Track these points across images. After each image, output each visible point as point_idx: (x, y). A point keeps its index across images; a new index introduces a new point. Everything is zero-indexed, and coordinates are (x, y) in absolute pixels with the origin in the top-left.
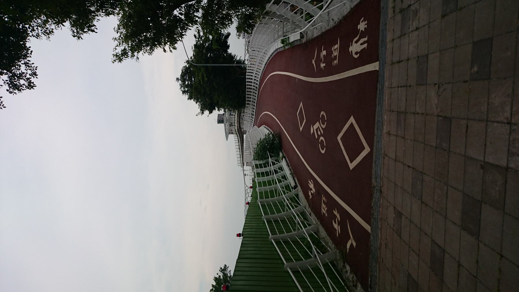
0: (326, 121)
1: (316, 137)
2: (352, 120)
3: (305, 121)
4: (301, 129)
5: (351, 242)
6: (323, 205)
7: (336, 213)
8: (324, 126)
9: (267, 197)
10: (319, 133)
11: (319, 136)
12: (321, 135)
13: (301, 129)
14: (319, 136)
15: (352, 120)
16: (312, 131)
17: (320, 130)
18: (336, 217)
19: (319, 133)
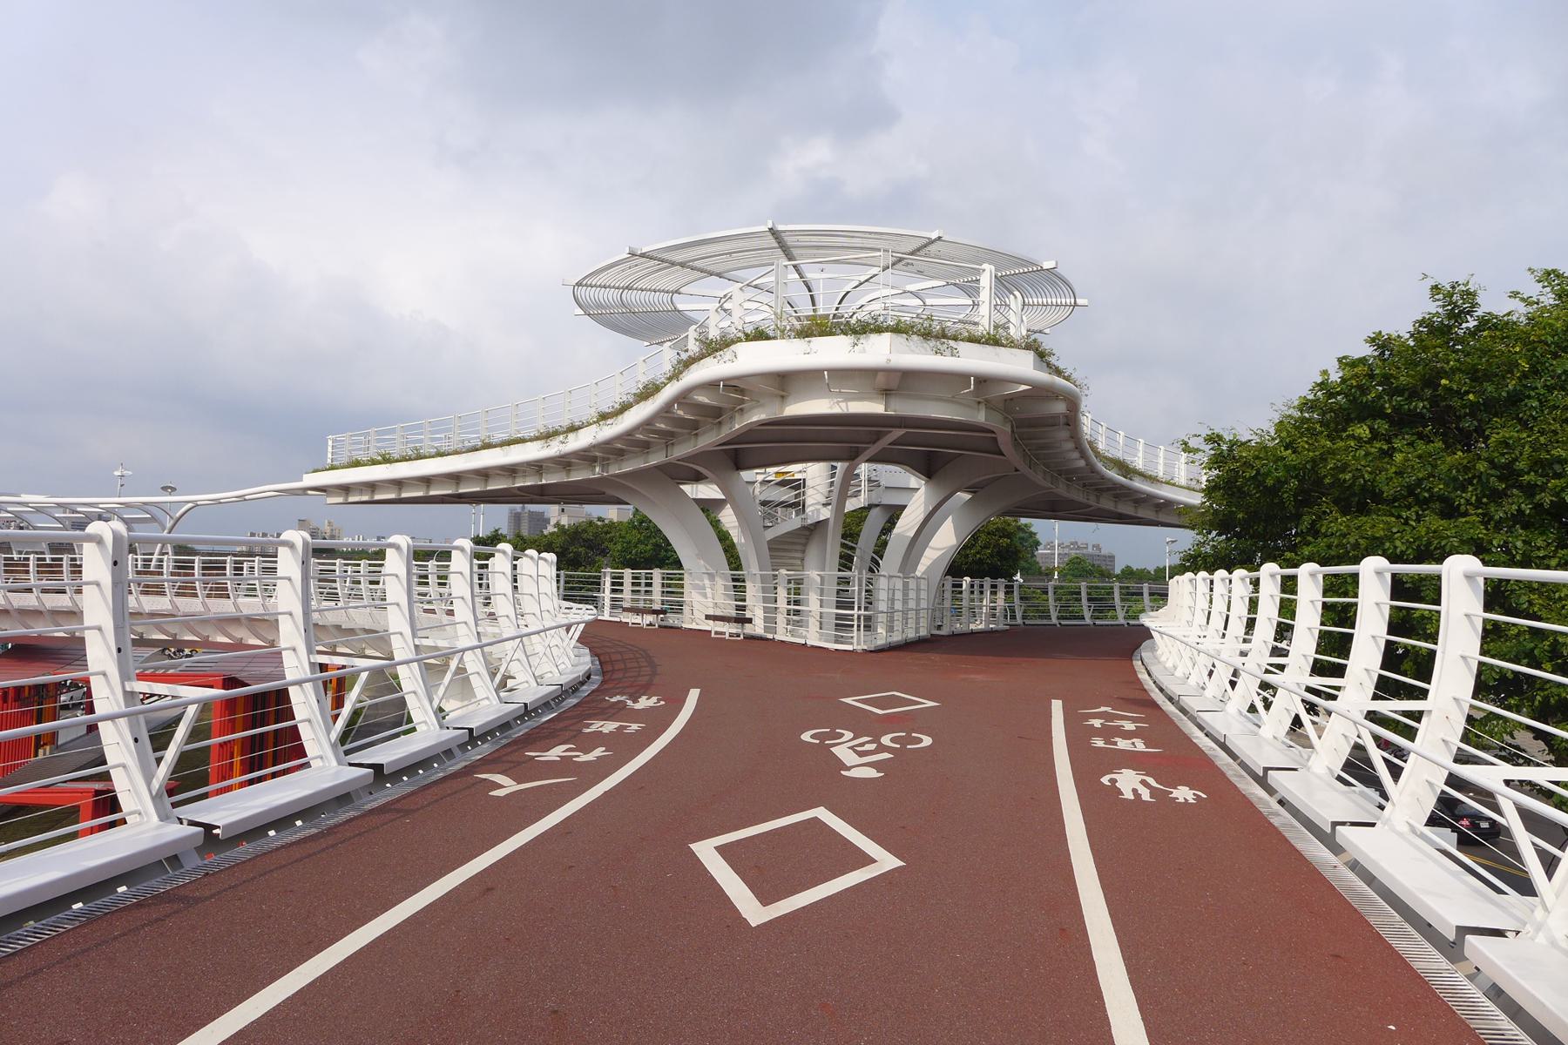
0: (909, 734)
1: (886, 756)
2: (886, 861)
3: (822, 813)
4: (848, 700)
5: (506, 785)
6: (617, 724)
7: (599, 752)
8: (848, 735)
9: (639, 584)
10: (872, 747)
11: (882, 748)
12: (876, 740)
13: (848, 700)
14: (882, 748)
15: (886, 861)
16: (872, 773)
17: (862, 745)
18: (586, 752)
19: (872, 747)
